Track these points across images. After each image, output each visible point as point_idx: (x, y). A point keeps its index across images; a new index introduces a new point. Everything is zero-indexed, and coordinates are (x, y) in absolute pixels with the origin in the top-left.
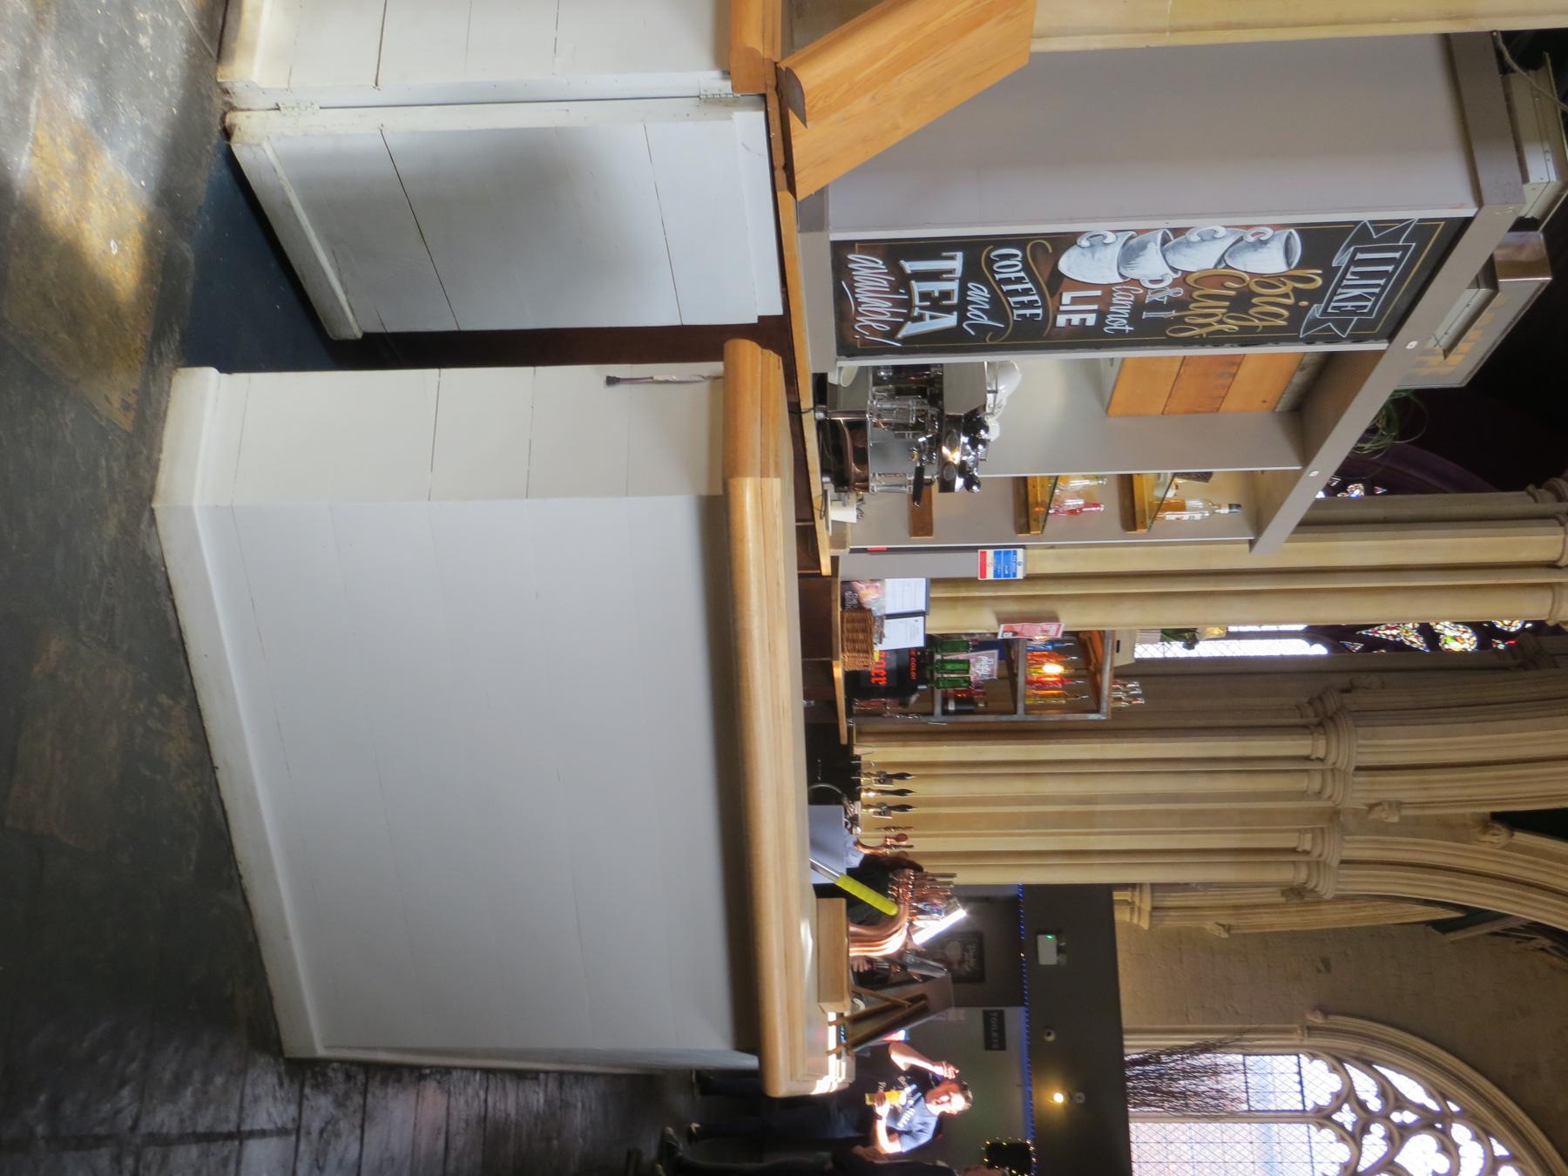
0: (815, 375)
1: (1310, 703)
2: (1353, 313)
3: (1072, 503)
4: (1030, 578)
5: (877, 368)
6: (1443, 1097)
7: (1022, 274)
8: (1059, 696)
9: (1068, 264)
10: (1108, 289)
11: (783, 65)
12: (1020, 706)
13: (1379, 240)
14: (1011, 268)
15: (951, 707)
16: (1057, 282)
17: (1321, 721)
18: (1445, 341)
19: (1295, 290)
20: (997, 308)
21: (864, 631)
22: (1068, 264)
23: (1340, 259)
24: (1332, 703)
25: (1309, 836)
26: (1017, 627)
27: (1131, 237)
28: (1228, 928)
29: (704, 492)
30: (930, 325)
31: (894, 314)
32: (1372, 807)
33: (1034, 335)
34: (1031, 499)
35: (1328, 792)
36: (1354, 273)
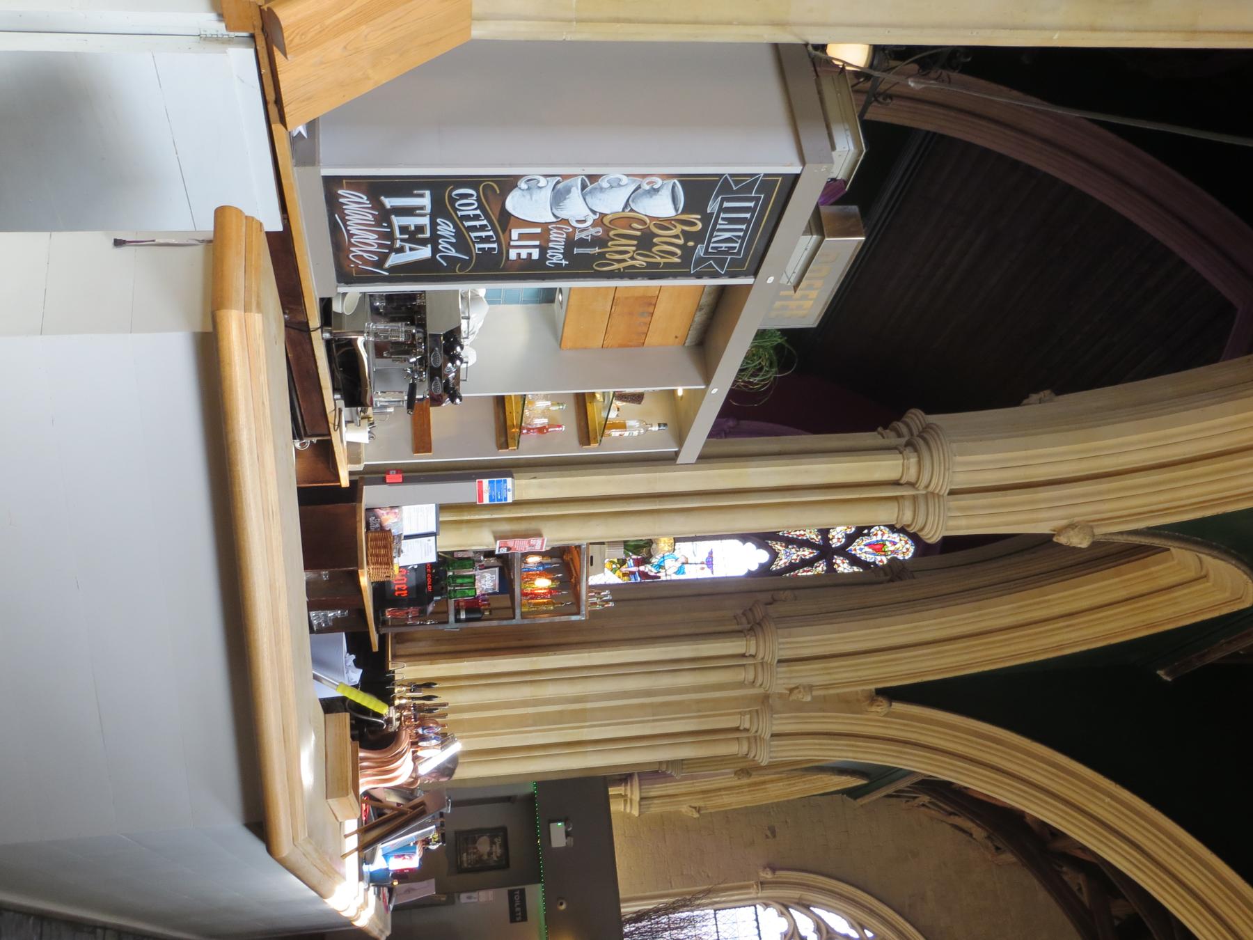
0: (322, 300)
1: (744, 614)
2: (727, 252)
3: (539, 422)
4: (517, 504)
5: (372, 296)
6: (861, 927)
7: (478, 212)
8: (548, 603)
9: (515, 203)
10: (545, 226)
11: (265, 7)
12: (518, 612)
13: (737, 192)
14: (469, 207)
15: (463, 616)
16: (506, 220)
17: (751, 626)
18: (793, 279)
19: (683, 232)
20: (461, 242)
21: (385, 547)
22: (515, 203)
23: (713, 207)
24: (759, 612)
25: (748, 717)
26: (510, 543)
27: (558, 183)
28: (698, 810)
29: (199, 330)
30: (409, 256)
31: (380, 246)
32: (791, 690)
33: (492, 267)
34: (509, 423)
35: (760, 681)
36: (723, 219)
